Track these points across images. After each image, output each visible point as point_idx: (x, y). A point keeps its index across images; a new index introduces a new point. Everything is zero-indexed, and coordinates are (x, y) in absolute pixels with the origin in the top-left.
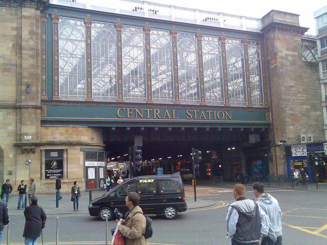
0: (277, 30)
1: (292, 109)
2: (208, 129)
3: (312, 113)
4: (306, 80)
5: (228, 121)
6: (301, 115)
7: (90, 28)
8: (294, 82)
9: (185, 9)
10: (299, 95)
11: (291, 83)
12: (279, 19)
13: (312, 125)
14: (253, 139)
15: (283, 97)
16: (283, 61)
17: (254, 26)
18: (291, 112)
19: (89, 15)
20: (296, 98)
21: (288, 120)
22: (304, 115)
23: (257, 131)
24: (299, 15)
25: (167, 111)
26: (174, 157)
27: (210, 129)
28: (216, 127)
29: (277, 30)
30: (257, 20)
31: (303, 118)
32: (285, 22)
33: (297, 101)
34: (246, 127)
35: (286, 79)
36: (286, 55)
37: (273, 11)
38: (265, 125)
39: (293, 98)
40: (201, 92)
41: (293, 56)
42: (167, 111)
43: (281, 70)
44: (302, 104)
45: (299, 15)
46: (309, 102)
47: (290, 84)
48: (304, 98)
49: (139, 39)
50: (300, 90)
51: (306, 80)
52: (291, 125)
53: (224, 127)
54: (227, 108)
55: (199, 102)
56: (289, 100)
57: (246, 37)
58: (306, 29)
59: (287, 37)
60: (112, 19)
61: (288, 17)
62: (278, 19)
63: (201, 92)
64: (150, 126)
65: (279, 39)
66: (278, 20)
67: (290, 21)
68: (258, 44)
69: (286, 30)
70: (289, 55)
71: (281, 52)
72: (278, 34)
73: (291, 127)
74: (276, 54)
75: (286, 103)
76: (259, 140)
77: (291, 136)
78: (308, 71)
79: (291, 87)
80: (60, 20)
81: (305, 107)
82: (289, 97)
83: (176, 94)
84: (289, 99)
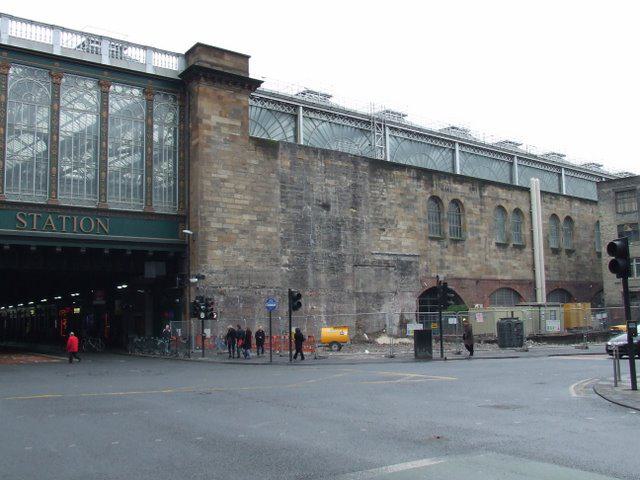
0: (202, 79)
1: (222, 220)
2: (33, 248)
3: (260, 229)
4: (252, 171)
5: (103, 236)
6: (237, 231)
7: (107, 93)
8: (229, 173)
9: (32, 22)
10: (238, 196)
11: (224, 174)
12: (210, 60)
13: (258, 250)
14: (152, 271)
15: (205, 198)
16: (212, 133)
17: (172, 66)
18: (219, 226)
19: (106, 73)
20: (231, 200)
21: (213, 239)
22: (243, 232)
23: (159, 256)
24: (248, 57)
25: (50, 217)
26: (26, 305)
27: (38, 247)
28: (28, 243)
29: (202, 79)
30: (178, 55)
31: (241, 236)
32: (222, 66)
33: (233, 206)
34: (14, 242)
35: (215, 166)
36: (218, 123)
37: (198, 45)
38: (177, 245)
39: (226, 200)
40: (101, 183)
41: (231, 127)
42: (50, 217)
43: (207, 150)
44: (243, 212)
45: (248, 57)
46: (256, 209)
47: (222, 176)
48: (247, 202)
49: (92, 99)
50: (240, 187)
51: (252, 171)
52: (217, 248)
53: (115, 247)
54: (102, 212)
55: (95, 202)
56: (217, 204)
57: (152, 83)
58: (259, 83)
59: (223, 93)
60: (83, 69)
61: (227, 57)
62: (206, 60)
63: (101, 183)
64: (120, 247)
65: (206, 95)
66: (207, 63)
67: (230, 65)
68: (175, 99)
69: (220, 81)
70: (224, 125)
71: (209, 117)
72: (203, 87)
73: (218, 252)
74: (199, 121)
75: (211, 209)
76: (164, 273)
77: (216, 267)
78: (260, 155)
79: (224, 180)
80: (64, 80)
81: (246, 217)
82: (217, 199)
83: (53, 179)
84: (217, 203)
